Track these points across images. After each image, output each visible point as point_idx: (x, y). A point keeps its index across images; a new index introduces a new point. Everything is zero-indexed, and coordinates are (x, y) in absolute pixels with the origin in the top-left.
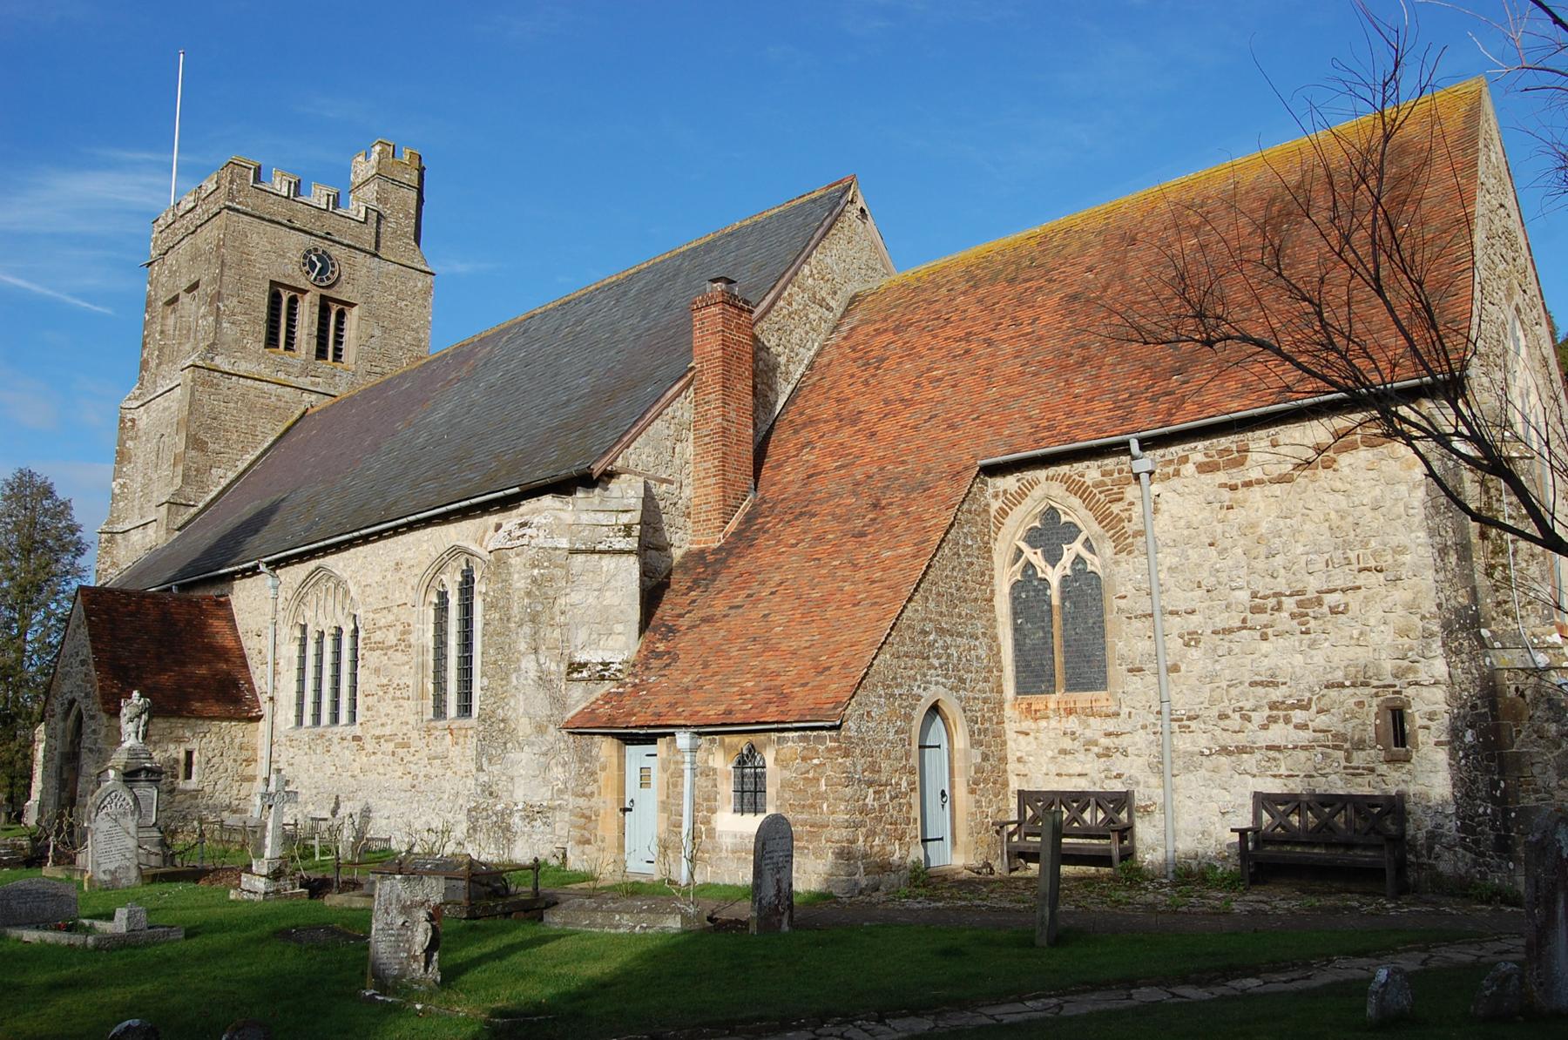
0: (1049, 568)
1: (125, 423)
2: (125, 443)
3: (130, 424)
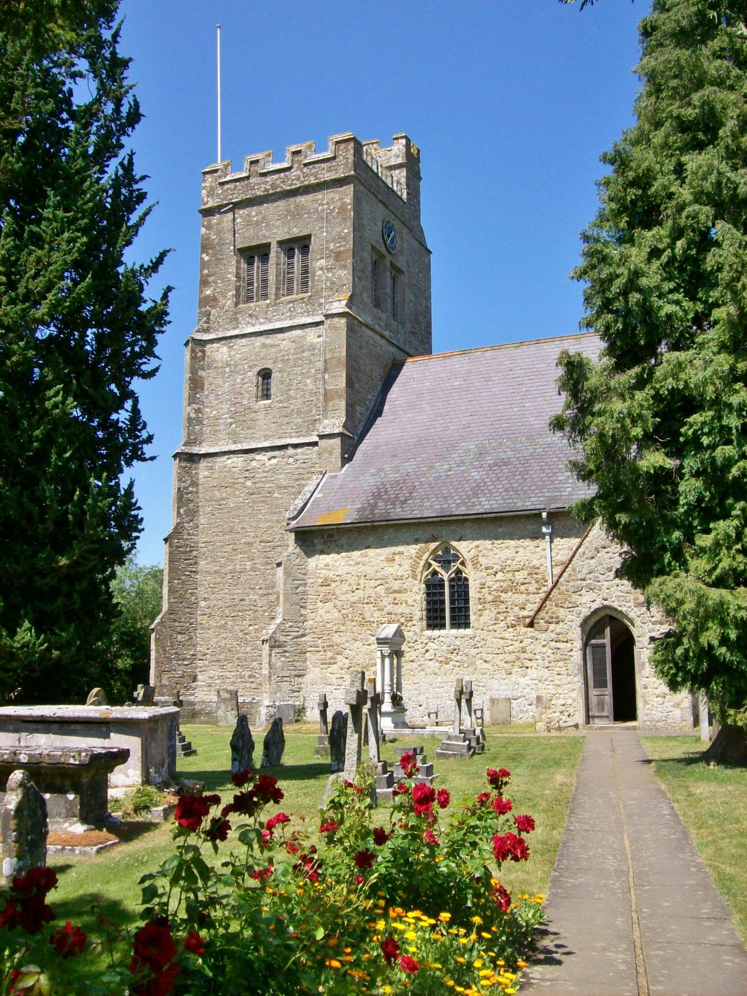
0: (443, 572)
1: (196, 354)
2: (197, 371)
3: (200, 354)
